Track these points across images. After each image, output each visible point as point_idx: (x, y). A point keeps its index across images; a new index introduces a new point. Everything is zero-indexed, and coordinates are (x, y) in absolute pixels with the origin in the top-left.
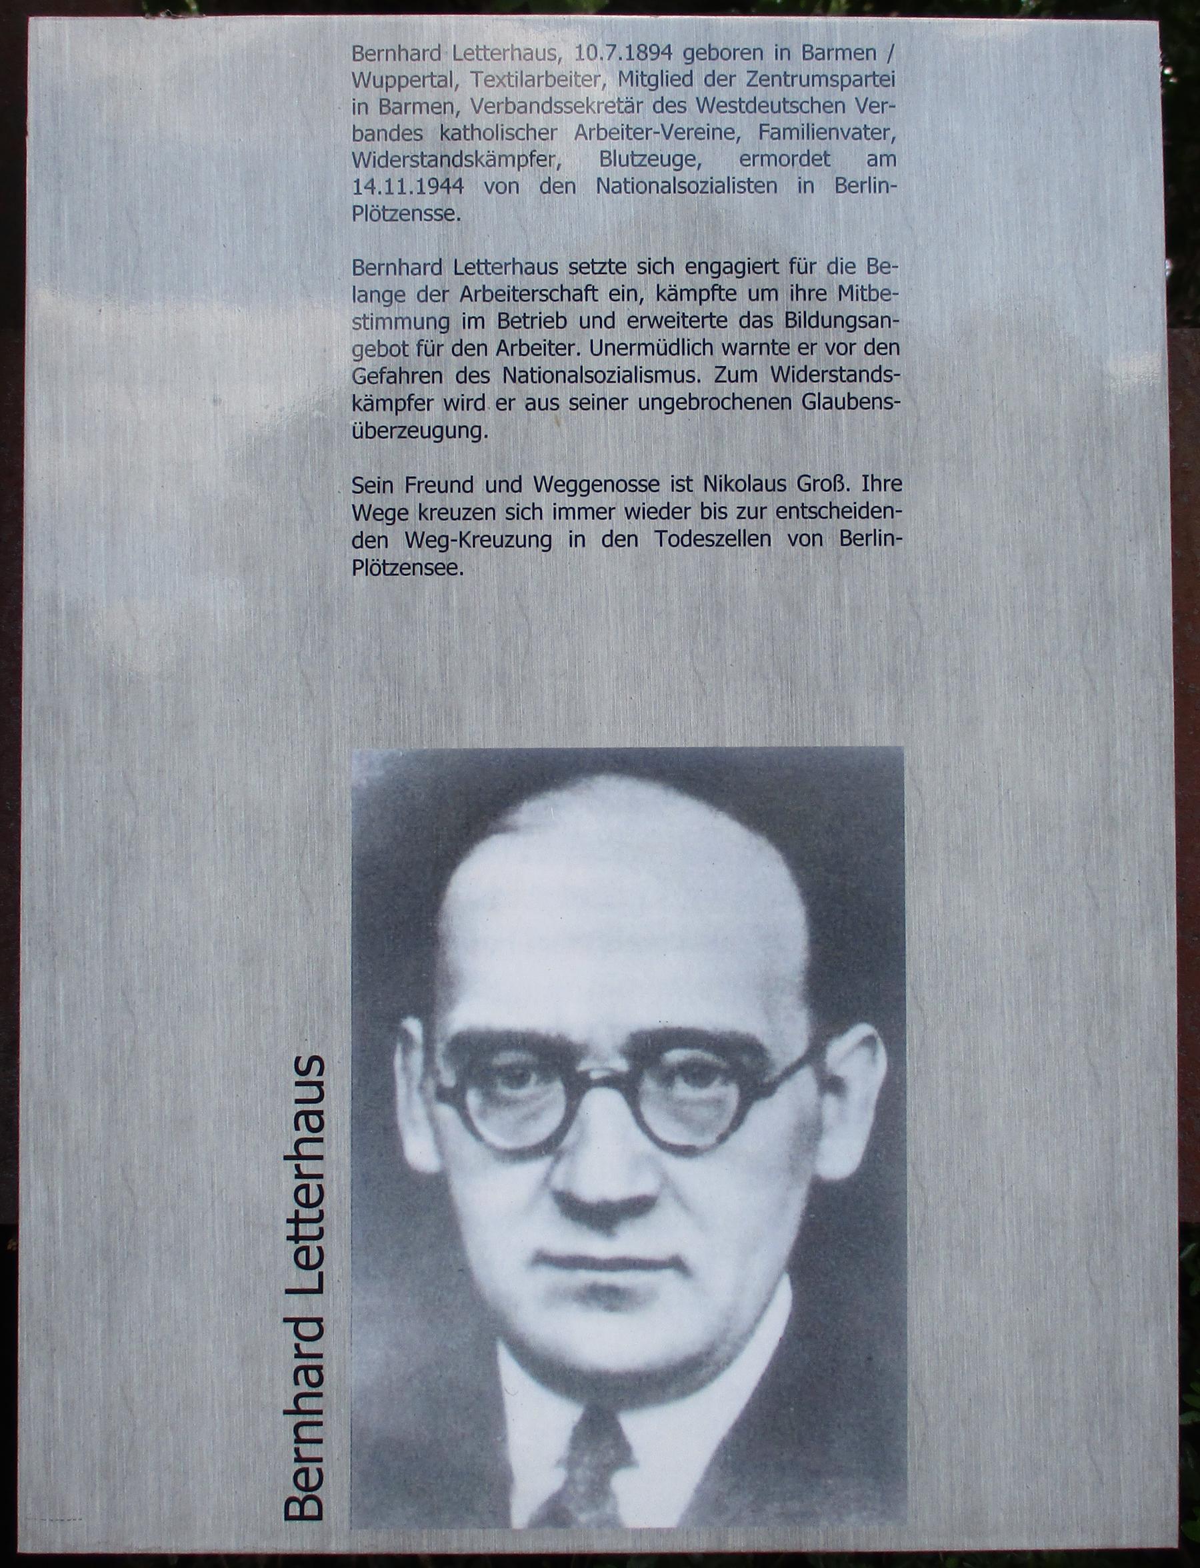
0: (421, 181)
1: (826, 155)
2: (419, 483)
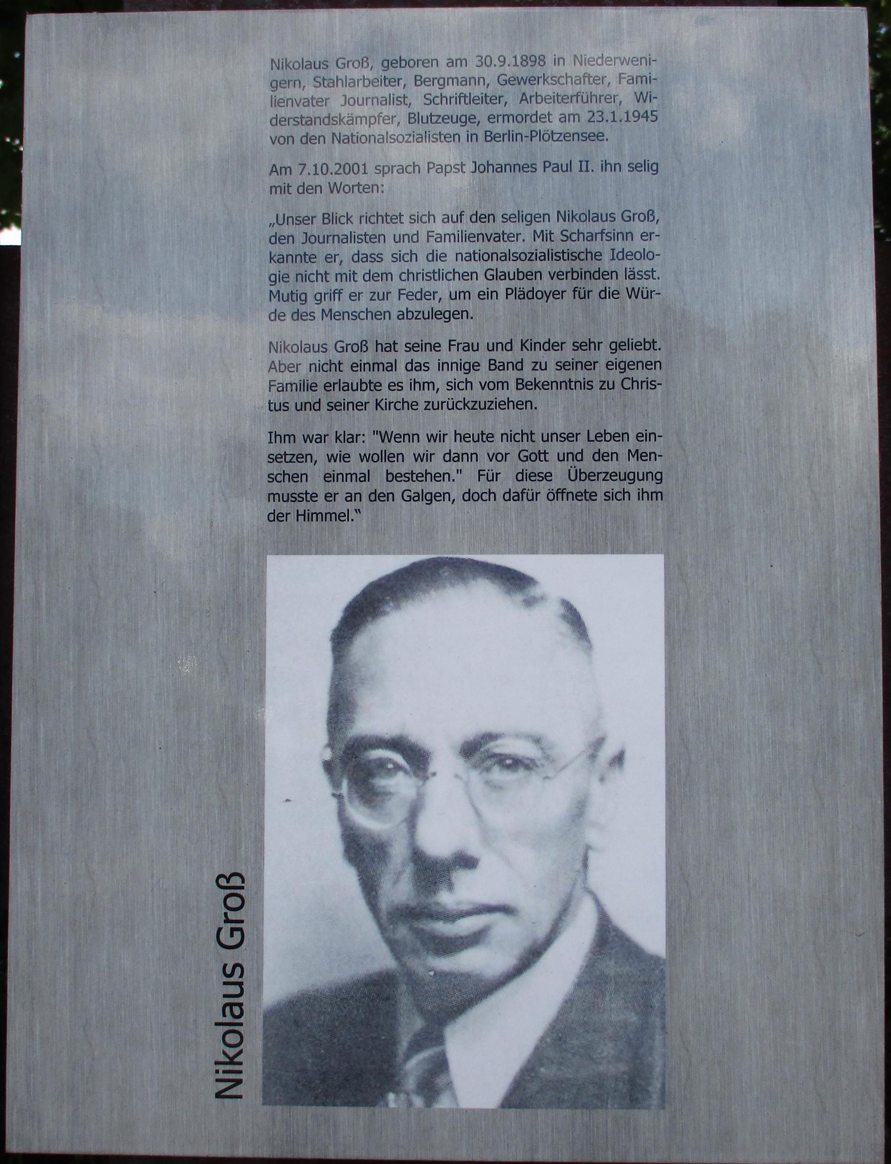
0: (627, 113)
1: (549, 114)
2: (458, 344)
